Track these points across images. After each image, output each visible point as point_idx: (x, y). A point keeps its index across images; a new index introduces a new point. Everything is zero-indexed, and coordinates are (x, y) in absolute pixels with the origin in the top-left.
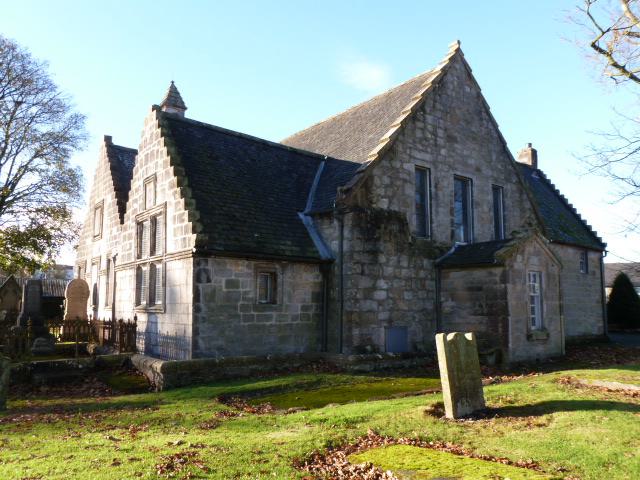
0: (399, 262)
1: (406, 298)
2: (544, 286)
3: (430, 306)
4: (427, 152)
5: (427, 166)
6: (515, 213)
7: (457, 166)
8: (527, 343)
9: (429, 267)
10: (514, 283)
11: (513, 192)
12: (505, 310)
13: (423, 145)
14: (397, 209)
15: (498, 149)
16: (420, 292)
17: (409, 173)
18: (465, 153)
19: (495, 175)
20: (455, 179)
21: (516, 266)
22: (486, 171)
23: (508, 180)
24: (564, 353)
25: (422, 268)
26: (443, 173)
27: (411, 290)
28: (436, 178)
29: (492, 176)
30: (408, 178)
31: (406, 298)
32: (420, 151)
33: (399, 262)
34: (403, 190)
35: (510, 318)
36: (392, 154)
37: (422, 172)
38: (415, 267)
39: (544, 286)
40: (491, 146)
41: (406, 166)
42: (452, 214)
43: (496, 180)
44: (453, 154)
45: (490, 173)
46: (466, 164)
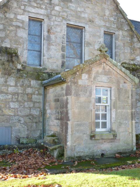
0: (6, 82)
1: (12, 106)
2: (113, 98)
3: (36, 112)
4: (42, 8)
5: (42, 17)
6: (126, 51)
7: (70, 18)
8: (90, 141)
9: (37, 86)
10: (77, 95)
11: (124, 36)
12: (68, 119)
13: (37, 4)
14: (9, 46)
15: (112, 7)
16: (26, 103)
17: (23, 22)
18: (79, 9)
19: (107, 25)
20: (67, 26)
21: (80, 82)
22: (98, 21)
23: (120, 28)
24: (135, 149)
25: (30, 86)
26: (56, 23)
27: (17, 101)
28: (48, 26)
29: (105, 26)
30: (21, 25)
31: (12, 106)
32: (34, 7)
33: (6, 82)
34: (16, 34)
35: (69, 123)
36: (6, 9)
37: (36, 21)
38: (22, 86)
39: (113, 98)
40: (105, 6)
41: (19, 17)
42: (63, 51)
43: (108, 28)
44: (67, 10)
45: (103, 23)
46: (79, 17)
